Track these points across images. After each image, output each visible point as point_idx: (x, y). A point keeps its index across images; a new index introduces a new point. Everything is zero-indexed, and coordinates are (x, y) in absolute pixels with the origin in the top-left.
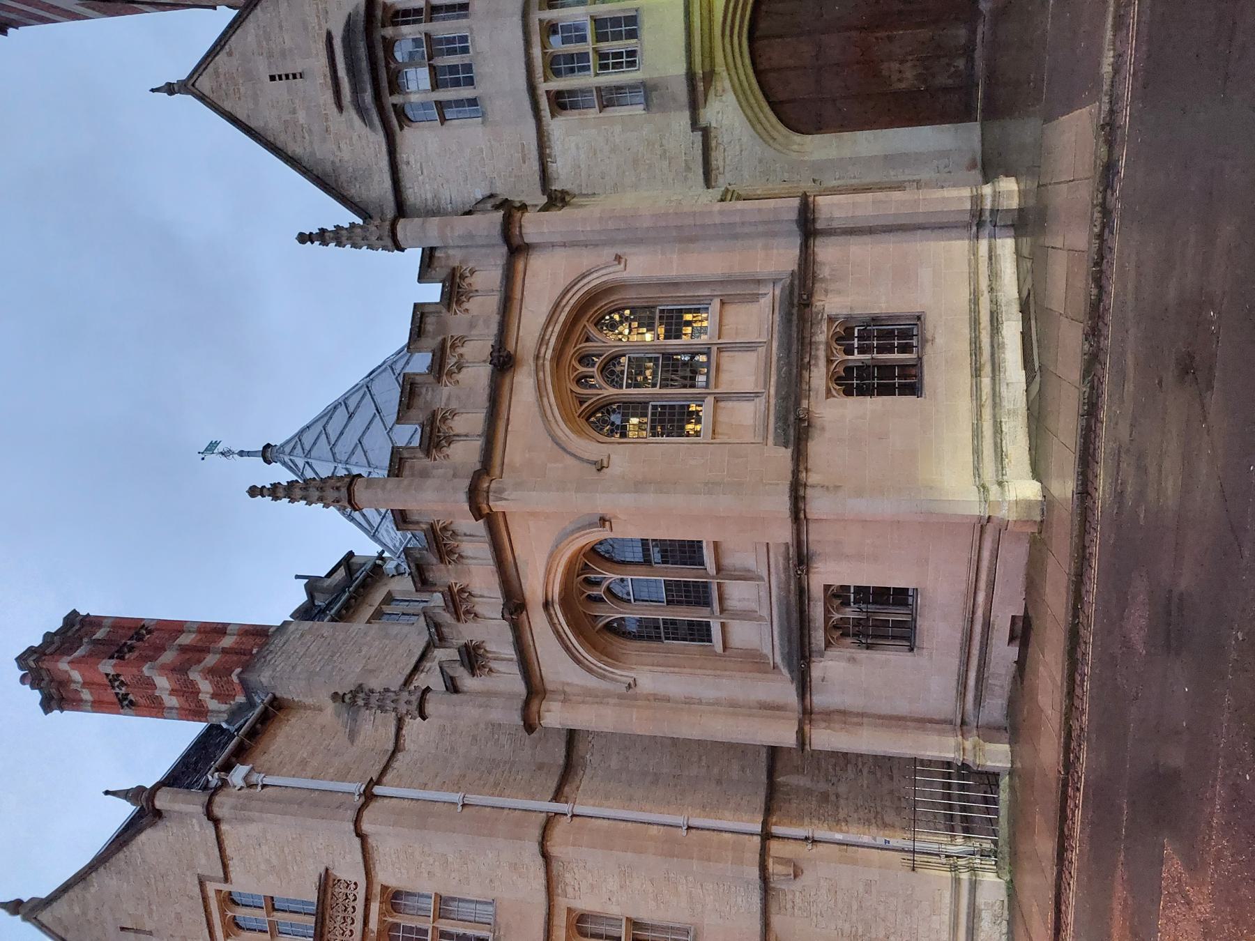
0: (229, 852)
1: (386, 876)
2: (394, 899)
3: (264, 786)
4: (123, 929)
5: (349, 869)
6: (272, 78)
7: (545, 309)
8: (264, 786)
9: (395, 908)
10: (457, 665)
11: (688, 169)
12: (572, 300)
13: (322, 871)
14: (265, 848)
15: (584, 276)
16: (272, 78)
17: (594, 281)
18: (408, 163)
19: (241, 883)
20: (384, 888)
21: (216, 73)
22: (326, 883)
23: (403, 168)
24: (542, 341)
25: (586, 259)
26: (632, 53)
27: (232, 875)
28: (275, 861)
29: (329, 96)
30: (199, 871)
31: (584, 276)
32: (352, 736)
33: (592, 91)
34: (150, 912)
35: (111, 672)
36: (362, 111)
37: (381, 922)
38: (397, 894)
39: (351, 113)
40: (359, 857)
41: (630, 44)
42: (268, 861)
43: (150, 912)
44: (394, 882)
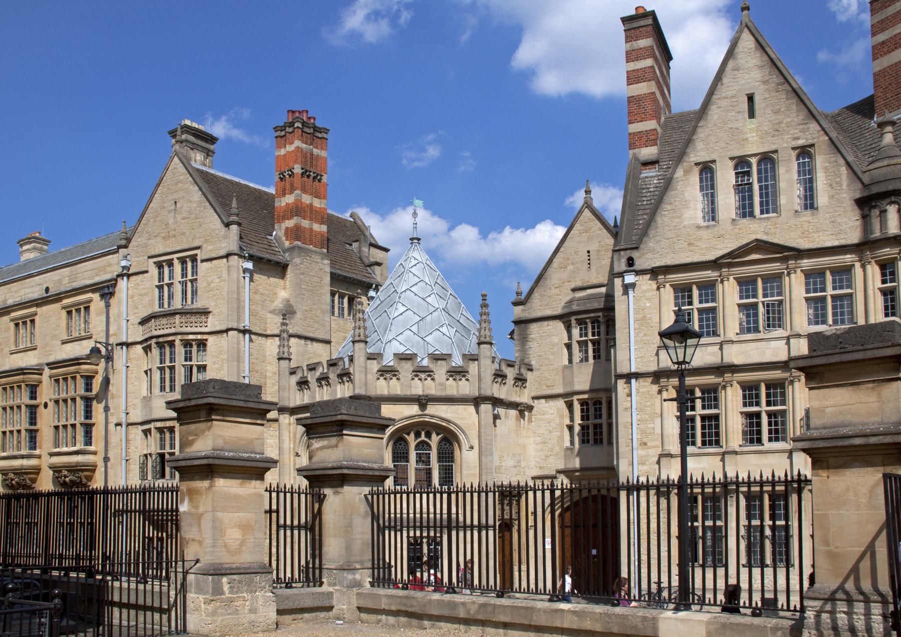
0: (214, 262)
1: (211, 340)
2: (202, 344)
3: (244, 277)
4: (176, 202)
5: (213, 323)
6: (588, 252)
7: (443, 415)
8: (244, 277)
9: (198, 346)
10: (301, 375)
11: (541, 468)
12: (452, 427)
13: (210, 310)
14: (218, 280)
15: (463, 432)
16: (588, 252)
17: (462, 437)
18: (548, 325)
19: (202, 267)
20: (206, 340)
21: (592, 221)
22: (205, 313)
23: (546, 323)
24: (432, 416)
25: (473, 434)
26: (588, 442)
27: (205, 264)
28: (212, 285)
29: (579, 283)
30: (205, 246)
31: (463, 432)
32: (272, 312)
33: (892, 281)
34: (184, 219)
35: (295, 171)
36: (570, 302)
37: (193, 340)
38: (205, 345)
39: (570, 296)
40: (218, 328)
41: (591, 441)
42: (212, 282)
43: (184, 219)
44: (209, 344)
